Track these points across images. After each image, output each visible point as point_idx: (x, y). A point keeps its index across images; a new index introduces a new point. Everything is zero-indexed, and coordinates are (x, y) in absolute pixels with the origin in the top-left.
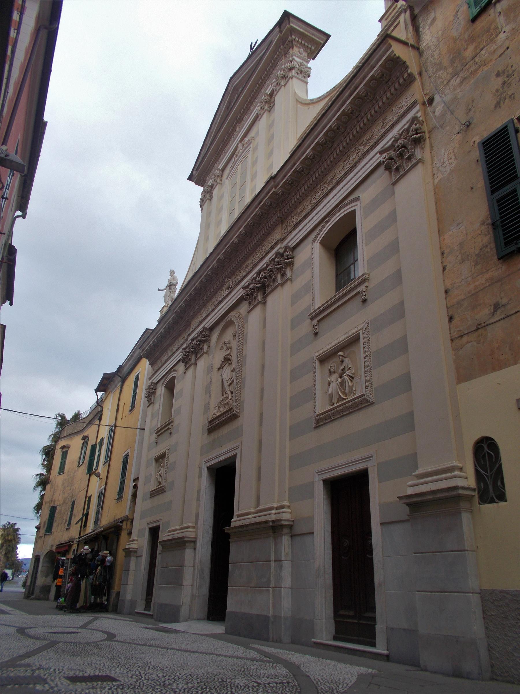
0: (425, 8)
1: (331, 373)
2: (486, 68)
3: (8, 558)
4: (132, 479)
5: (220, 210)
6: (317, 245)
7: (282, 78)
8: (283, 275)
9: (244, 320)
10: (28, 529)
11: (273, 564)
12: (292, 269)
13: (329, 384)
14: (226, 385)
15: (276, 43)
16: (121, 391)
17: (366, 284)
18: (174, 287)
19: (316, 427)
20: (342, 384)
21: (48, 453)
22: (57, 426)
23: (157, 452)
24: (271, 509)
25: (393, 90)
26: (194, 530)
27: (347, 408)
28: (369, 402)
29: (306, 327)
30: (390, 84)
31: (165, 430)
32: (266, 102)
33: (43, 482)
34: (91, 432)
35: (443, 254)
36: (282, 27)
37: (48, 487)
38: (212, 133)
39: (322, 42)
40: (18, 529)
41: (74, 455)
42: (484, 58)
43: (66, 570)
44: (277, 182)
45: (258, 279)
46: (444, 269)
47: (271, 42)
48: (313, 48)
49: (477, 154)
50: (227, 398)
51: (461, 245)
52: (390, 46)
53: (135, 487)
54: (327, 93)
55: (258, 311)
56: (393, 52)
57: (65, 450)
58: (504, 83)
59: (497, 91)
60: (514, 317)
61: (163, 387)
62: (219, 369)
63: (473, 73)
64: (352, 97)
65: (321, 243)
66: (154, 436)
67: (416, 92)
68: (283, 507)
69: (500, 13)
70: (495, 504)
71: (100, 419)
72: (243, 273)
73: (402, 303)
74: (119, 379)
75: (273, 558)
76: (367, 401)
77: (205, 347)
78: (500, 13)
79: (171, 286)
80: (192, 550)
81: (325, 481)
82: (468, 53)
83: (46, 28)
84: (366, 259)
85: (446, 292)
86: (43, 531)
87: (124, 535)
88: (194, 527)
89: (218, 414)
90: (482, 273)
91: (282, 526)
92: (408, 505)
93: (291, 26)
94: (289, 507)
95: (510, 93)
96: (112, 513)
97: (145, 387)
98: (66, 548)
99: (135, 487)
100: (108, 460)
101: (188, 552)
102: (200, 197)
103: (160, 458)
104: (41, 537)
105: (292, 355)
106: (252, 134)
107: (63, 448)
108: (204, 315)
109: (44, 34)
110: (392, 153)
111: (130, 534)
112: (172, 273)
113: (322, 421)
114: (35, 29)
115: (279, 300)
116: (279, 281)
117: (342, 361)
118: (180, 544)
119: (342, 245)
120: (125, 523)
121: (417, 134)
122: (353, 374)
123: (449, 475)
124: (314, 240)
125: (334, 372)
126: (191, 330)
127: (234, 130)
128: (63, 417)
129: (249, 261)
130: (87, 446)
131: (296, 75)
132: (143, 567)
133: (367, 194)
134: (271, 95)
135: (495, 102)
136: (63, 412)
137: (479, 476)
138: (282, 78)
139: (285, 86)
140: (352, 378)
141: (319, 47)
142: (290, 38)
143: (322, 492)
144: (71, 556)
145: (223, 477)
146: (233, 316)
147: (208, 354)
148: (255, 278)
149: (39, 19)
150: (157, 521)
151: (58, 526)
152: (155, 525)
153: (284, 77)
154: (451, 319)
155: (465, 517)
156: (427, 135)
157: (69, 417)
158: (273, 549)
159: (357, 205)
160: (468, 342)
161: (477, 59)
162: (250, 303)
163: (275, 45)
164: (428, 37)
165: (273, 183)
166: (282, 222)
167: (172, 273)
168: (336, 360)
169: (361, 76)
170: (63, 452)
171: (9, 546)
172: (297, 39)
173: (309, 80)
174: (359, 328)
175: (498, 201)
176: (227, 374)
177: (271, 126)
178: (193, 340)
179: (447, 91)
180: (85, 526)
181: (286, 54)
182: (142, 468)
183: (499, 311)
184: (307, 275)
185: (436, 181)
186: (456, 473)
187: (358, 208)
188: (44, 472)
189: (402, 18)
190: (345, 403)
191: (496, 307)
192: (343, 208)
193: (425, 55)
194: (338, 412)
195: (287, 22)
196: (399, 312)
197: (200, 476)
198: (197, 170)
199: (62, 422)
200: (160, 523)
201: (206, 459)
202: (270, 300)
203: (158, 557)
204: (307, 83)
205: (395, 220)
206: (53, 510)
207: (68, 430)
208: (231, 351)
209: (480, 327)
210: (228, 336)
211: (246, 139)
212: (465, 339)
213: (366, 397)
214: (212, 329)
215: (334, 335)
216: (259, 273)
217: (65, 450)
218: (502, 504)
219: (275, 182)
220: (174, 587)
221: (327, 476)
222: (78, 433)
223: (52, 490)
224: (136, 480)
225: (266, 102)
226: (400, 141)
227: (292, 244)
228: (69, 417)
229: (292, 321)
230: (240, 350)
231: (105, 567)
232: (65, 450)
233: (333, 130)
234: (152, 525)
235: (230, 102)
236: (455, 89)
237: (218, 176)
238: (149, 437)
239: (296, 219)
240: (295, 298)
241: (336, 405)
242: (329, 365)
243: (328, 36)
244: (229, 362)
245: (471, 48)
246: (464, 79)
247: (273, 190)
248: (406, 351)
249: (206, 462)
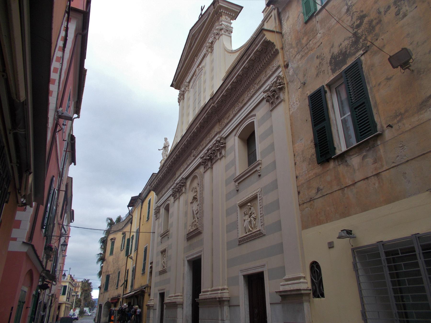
0: (284, 9)
1: (245, 215)
2: (312, 52)
3: (86, 300)
4: (149, 262)
5: (188, 107)
6: (237, 138)
7: (217, 34)
8: (220, 153)
9: (202, 177)
10: (97, 283)
11: (220, 322)
12: (225, 150)
13: (244, 221)
14: (195, 213)
16: (142, 208)
17: (260, 166)
19: (239, 245)
20: (250, 222)
21: (104, 241)
22: (108, 225)
23: (161, 248)
24: (218, 290)
25: (268, 57)
26: (182, 297)
27: (253, 236)
29: (233, 186)
31: (165, 235)
32: (209, 47)
33: (102, 259)
34: (127, 229)
35: (294, 155)
37: (105, 262)
39: (239, 11)
40: (90, 283)
41: (118, 243)
42: (311, 46)
43: (115, 317)
45: (208, 154)
46: (295, 164)
47: (210, 13)
48: (233, 15)
49: (307, 102)
50: (195, 221)
51: (303, 151)
52: (264, 35)
53: (151, 267)
55: (208, 172)
56: (266, 38)
57: (113, 241)
58: (320, 63)
59: (317, 67)
60: (326, 196)
61: (163, 209)
62: (191, 203)
63: (306, 54)
66: (160, 238)
67: (279, 60)
68: (224, 289)
69: (318, 22)
70: (319, 299)
71: (131, 223)
72: (201, 148)
73: (276, 180)
74: (140, 200)
75: (220, 319)
76: (262, 234)
77: (184, 189)
78: (318, 22)
79: (165, 147)
80: (181, 309)
81: (244, 276)
82: (304, 41)
83: (80, 34)
84: (260, 151)
85: (297, 177)
86: (103, 290)
87: (146, 295)
88: (181, 296)
89: (192, 230)
90: (312, 170)
91: (224, 301)
92: (281, 296)
94: (227, 289)
95: (323, 69)
96: (140, 282)
97: (154, 208)
98: (116, 301)
99: (151, 267)
100: (137, 249)
101: (179, 310)
102: (178, 97)
103: (163, 252)
104: (102, 293)
105: (226, 201)
106: (203, 64)
107: (112, 239)
108: (182, 170)
109: (80, 37)
110: (270, 94)
111: (149, 295)
112: (166, 139)
113: (242, 241)
114: (75, 36)
115: (219, 167)
116: (219, 156)
117: (250, 209)
118: (174, 305)
119: (249, 139)
120: (146, 288)
121: (280, 85)
122: (256, 217)
123: (298, 281)
124: (235, 135)
125: (247, 214)
126: (176, 177)
127: (193, 61)
128: (111, 220)
129: (204, 142)
130: (125, 239)
131: (224, 33)
132: (157, 316)
134: (212, 43)
135: (316, 73)
136: (111, 217)
137: (313, 283)
138: (217, 34)
140: (255, 219)
143: (243, 283)
144: (117, 308)
145: (196, 265)
146: (197, 173)
147: (185, 193)
148: (206, 153)
149: (76, 30)
150: (163, 290)
151: (111, 287)
152: (162, 291)
153: (218, 34)
154: (299, 193)
155: (306, 305)
156: (286, 85)
157: (114, 220)
158: (220, 313)
160: (306, 207)
161: (308, 46)
162: (204, 167)
164: (287, 27)
166: (219, 122)
167: (166, 139)
170: (112, 242)
171: (86, 293)
172: (224, 11)
173: (232, 35)
174: (258, 191)
175: (317, 131)
176: (195, 206)
177: (212, 61)
178: (177, 184)
179: (295, 62)
180: (126, 287)
181: (218, 19)
182: (154, 256)
183: (319, 192)
184: (233, 153)
185: (291, 112)
186: (302, 280)
187: (255, 120)
188: (102, 252)
189: (273, 14)
190: (252, 233)
191: (318, 190)
192: (248, 119)
193: (286, 37)
194: (249, 238)
195: (217, 2)
196: (274, 185)
197: (184, 266)
199: (111, 223)
200: (165, 291)
201: (186, 256)
202: (214, 166)
203: (165, 311)
204: (231, 37)
205: (272, 132)
206: (108, 277)
207: (114, 228)
209: (311, 200)
210: (195, 184)
211: (200, 67)
212: (305, 205)
214: (187, 178)
215: (246, 194)
216: (208, 150)
217: (113, 241)
218: (322, 299)
221: (245, 273)
222: (119, 230)
223: (107, 265)
224: (151, 263)
225: (209, 47)
226: (272, 88)
227: (224, 135)
228: (114, 220)
229: (226, 181)
230: (202, 194)
231: (137, 315)
232: (113, 241)
233: (240, 76)
234: (161, 292)
235: (191, 44)
236: (298, 62)
238: (157, 239)
239: (226, 121)
240: (227, 168)
241: (248, 233)
242: (245, 209)
245: (305, 39)
246: (302, 56)
247: (213, 105)
248: (278, 208)
249: (187, 257)
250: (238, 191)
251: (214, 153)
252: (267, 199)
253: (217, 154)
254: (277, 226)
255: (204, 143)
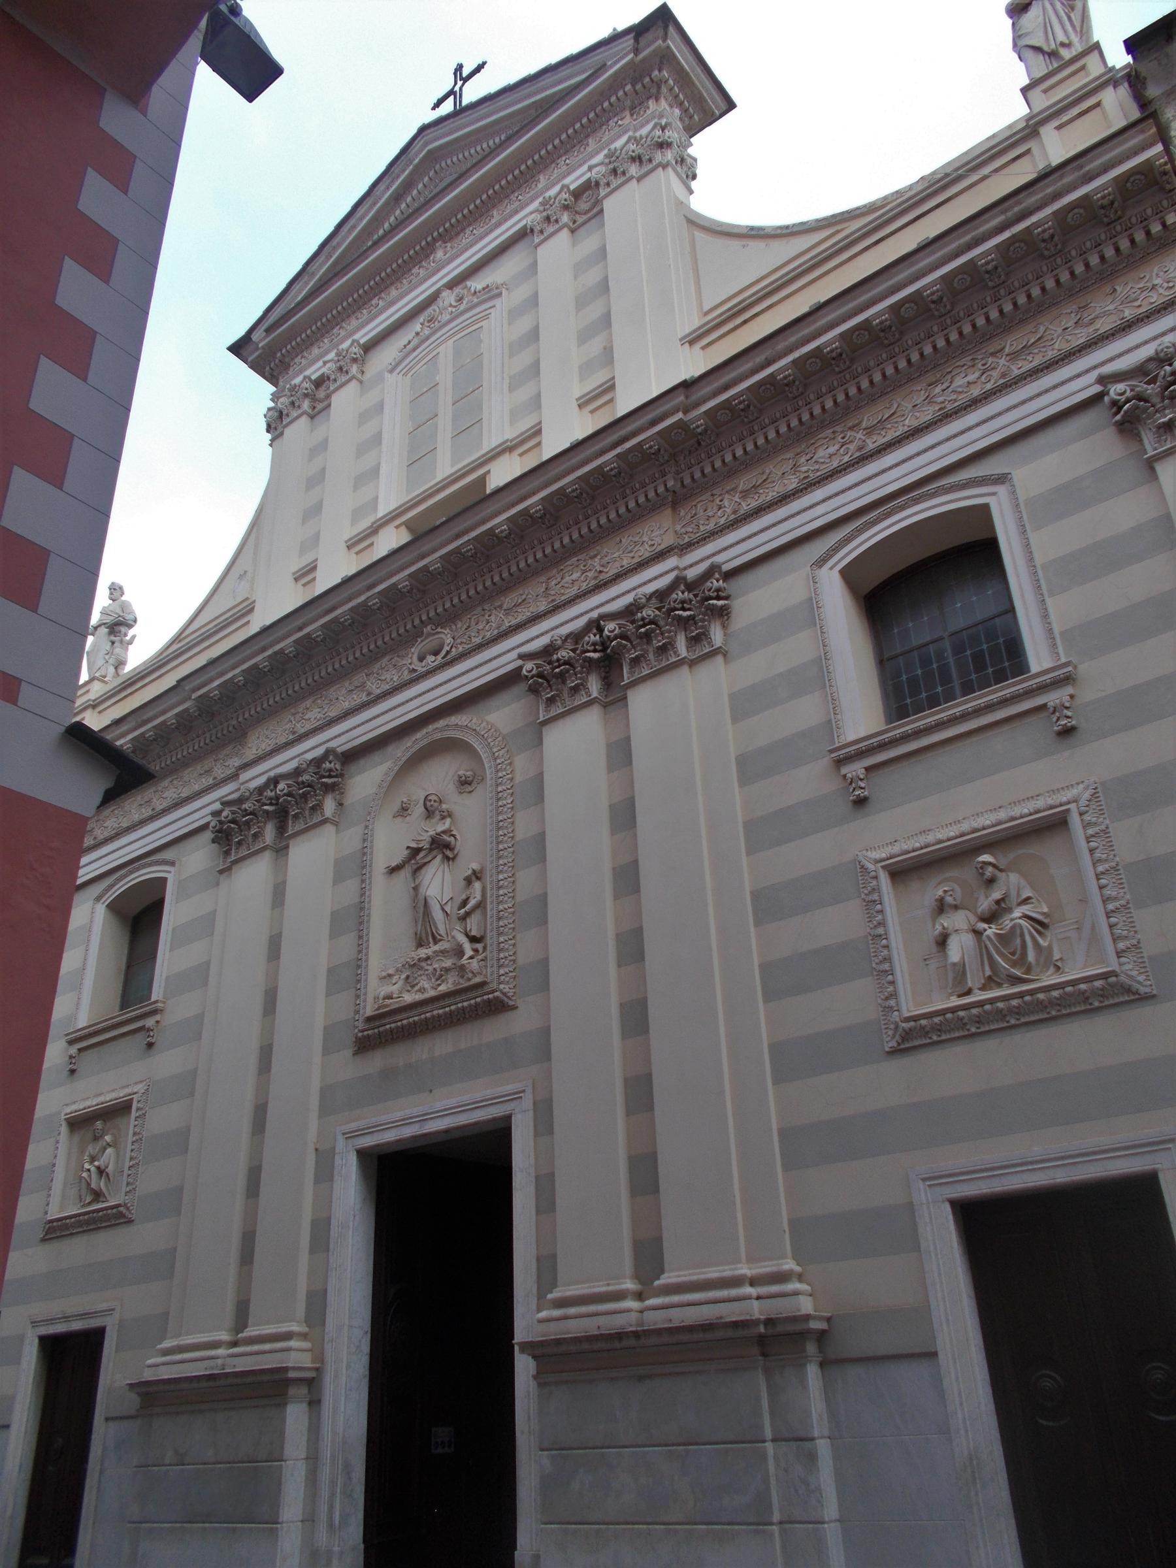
6: (101, 909)
15: (616, 73)
17: (158, 1017)
18: (123, 629)
19: (44, 1240)
28: (1137, 993)
30: (1118, 228)
36: (643, 41)
38: (335, 249)
44: (694, 398)
47: (603, 67)
54: (817, 220)
64: (1007, 235)
65: (842, 572)
75: (768, 1434)
77: (329, 806)
91: (804, 1335)
93: (668, 47)
94: (800, 1277)
101: (295, 1415)
127: (427, 251)
133: (1036, 472)
138: (633, 159)
139: (639, 180)
141: (709, 118)
142: (656, 73)
147: (336, 824)
159: (994, 494)
163: (611, 76)
165: (682, 398)
168: (965, 872)
169: (1049, 190)
173: (694, 185)
192: (150, 865)
195: (661, 32)
198: (268, 331)
201: (353, 1126)
208: (452, 823)
213: (1123, 978)
219: (687, 397)
220: (234, 1529)
227: (730, 559)
237: (355, 360)
239: (730, 504)
243: (731, 105)
244: (448, 853)
247: (680, 415)
250: (72, 1072)
251: (304, 797)
252: (161, 1119)
253: (263, 828)
254: (171, 1201)
255: (534, 597)
